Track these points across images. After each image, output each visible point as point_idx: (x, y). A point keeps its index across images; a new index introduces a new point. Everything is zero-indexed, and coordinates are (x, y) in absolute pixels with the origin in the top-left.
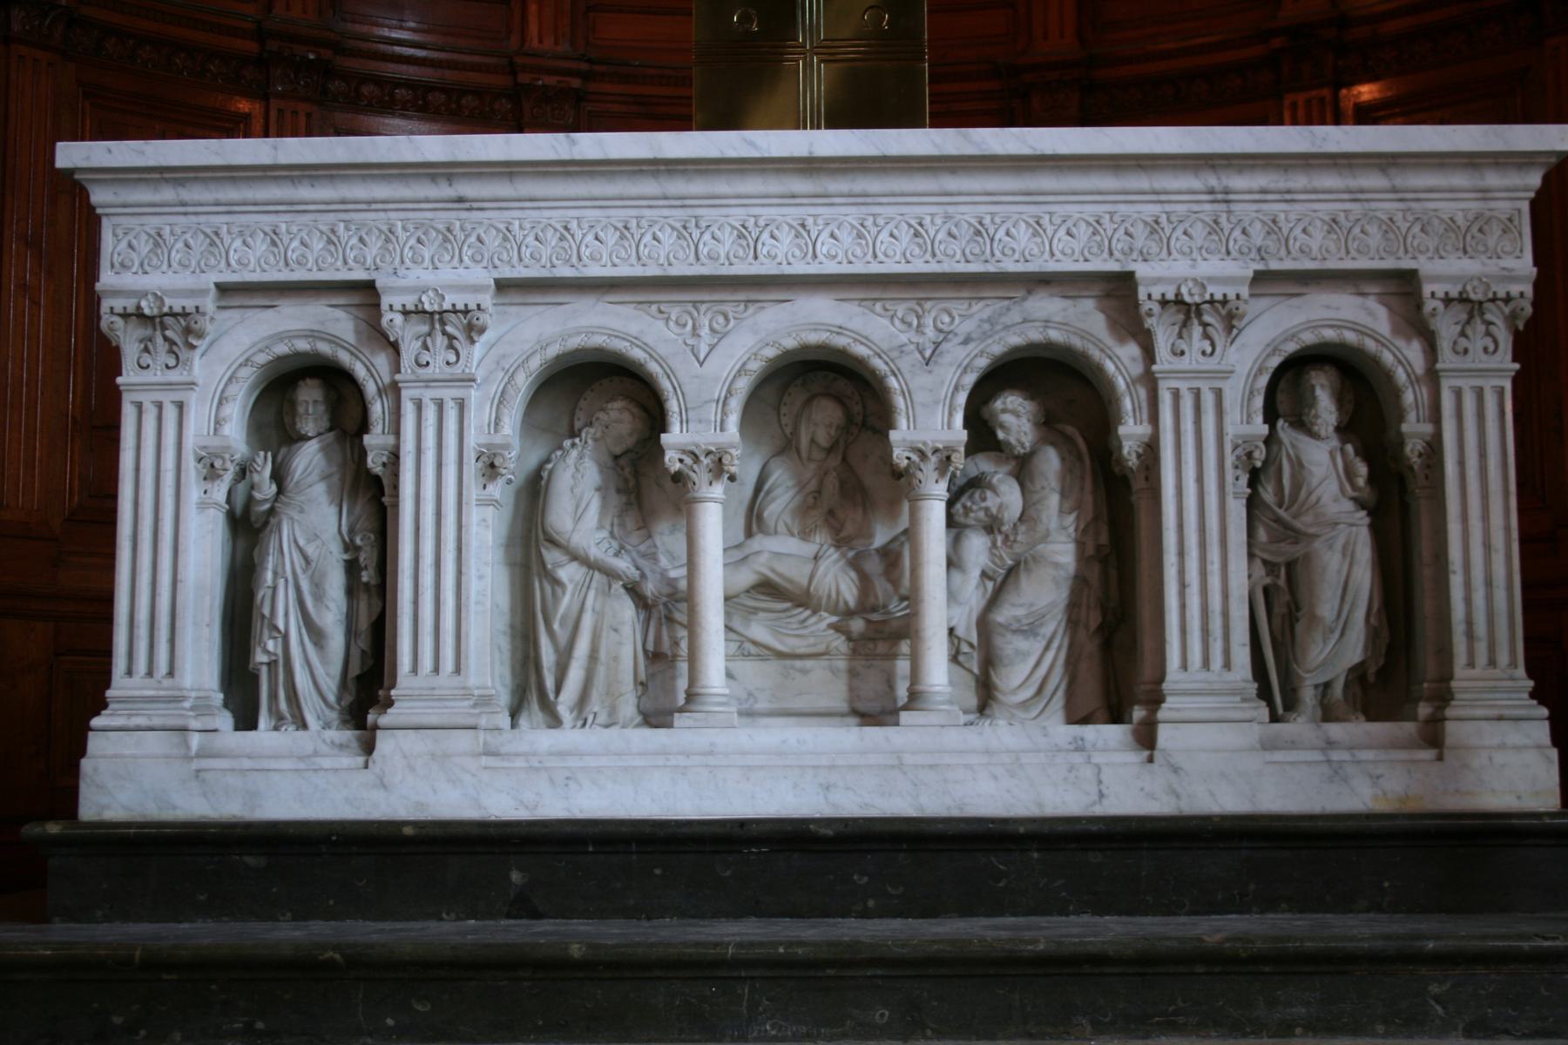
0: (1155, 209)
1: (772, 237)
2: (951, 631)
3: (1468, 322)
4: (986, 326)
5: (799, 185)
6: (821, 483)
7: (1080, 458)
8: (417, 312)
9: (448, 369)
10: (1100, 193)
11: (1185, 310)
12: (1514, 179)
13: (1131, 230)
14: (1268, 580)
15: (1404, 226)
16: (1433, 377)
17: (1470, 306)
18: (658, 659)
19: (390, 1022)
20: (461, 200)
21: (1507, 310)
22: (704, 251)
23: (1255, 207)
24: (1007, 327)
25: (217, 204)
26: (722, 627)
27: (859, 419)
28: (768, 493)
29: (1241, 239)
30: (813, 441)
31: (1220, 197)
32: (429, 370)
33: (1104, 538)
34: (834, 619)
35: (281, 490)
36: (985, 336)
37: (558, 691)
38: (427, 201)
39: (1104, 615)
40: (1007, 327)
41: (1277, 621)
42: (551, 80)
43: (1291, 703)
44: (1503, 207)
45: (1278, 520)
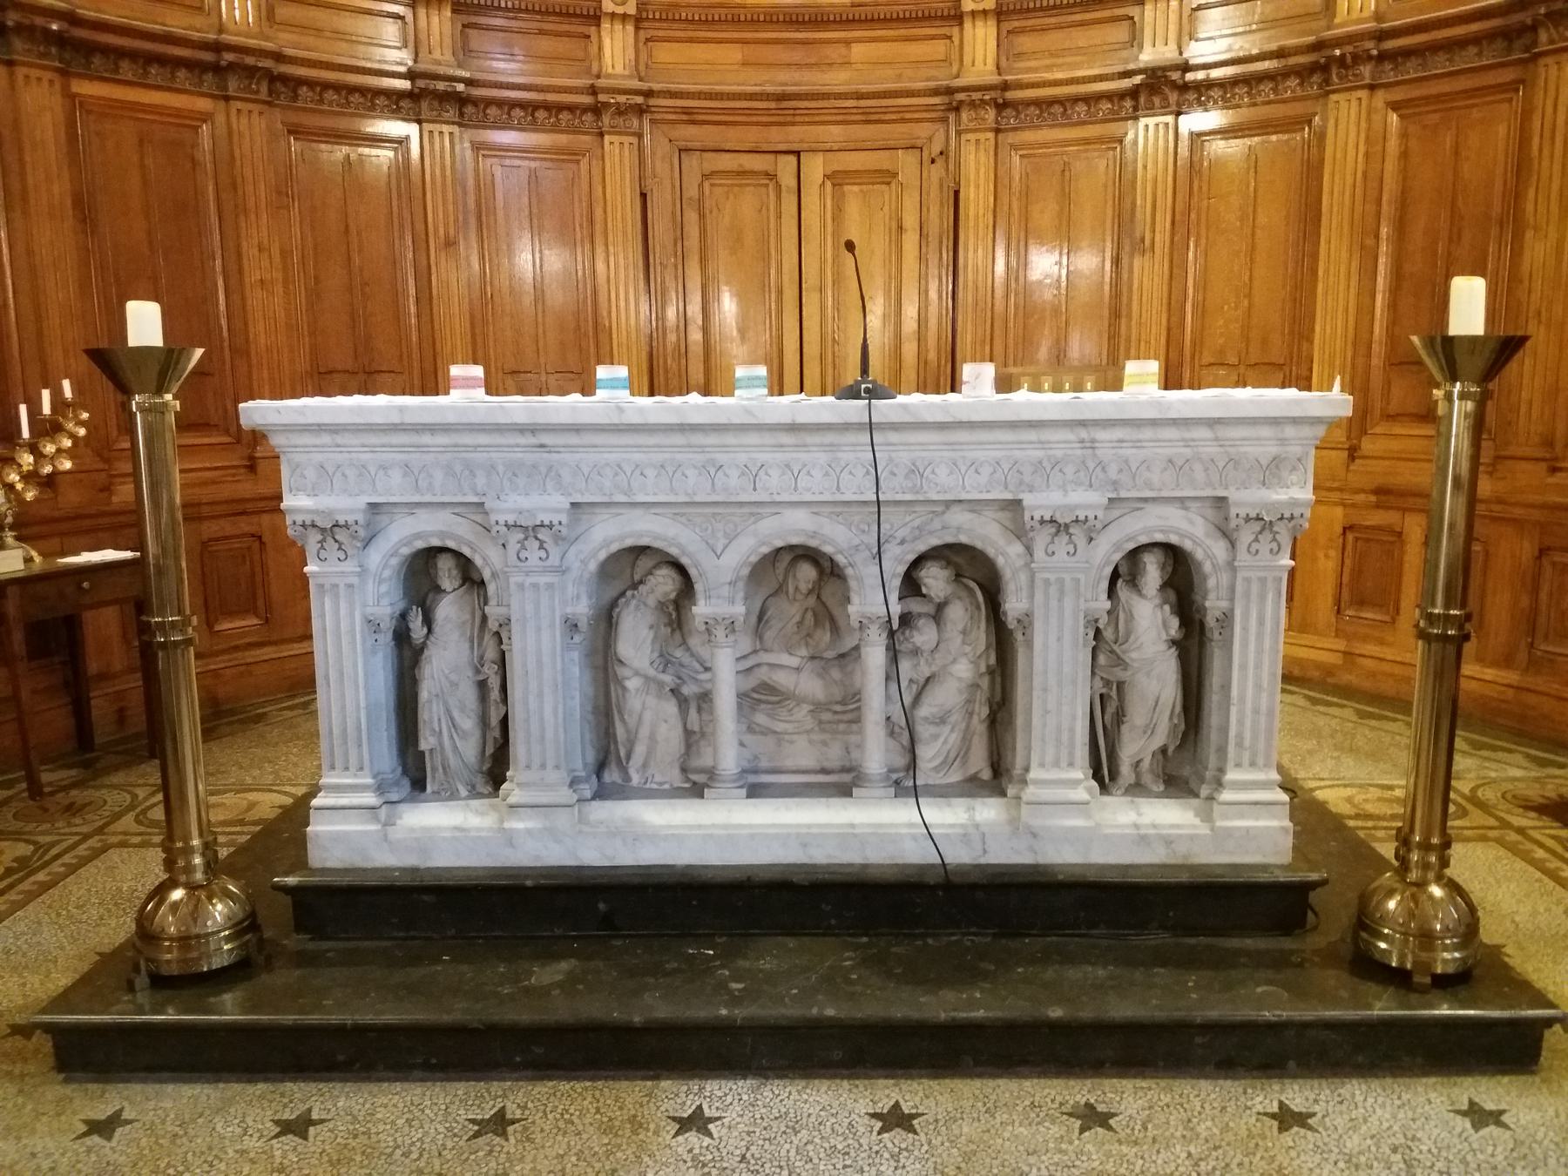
0: (1040, 454)
1: (767, 474)
2: (888, 718)
3: (1260, 532)
4: (917, 532)
5: (786, 439)
6: (803, 618)
7: (978, 608)
8: (515, 526)
9: (541, 563)
10: (1000, 443)
11: (1058, 527)
12: (1307, 431)
13: (1022, 469)
14: (1104, 691)
15: (1221, 464)
16: (1231, 566)
17: (1263, 524)
18: (691, 739)
19: (518, 1059)
20: (542, 446)
21: (1291, 525)
22: (718, 484)
23: (1114, 451)
24: (931, 533)
25: (364, 446)
26: (735, 743)
27: (828, 571)
28: (767, 622)
29: (1101, 475)
30: (797, 588)
31: (1088, 445)
32: (527, 563)
33: (993, 660)
34: (812, 707)
35: (430, 631)
36: (915, 539)
37: (629, 757)
38: (518, 446)
39: (990, 708)
40: (931, 533)
41: (1108, 717)
42: (622, 99)
43: (1114, 775)
44: (1295, 450)
45: (1112, 652)
